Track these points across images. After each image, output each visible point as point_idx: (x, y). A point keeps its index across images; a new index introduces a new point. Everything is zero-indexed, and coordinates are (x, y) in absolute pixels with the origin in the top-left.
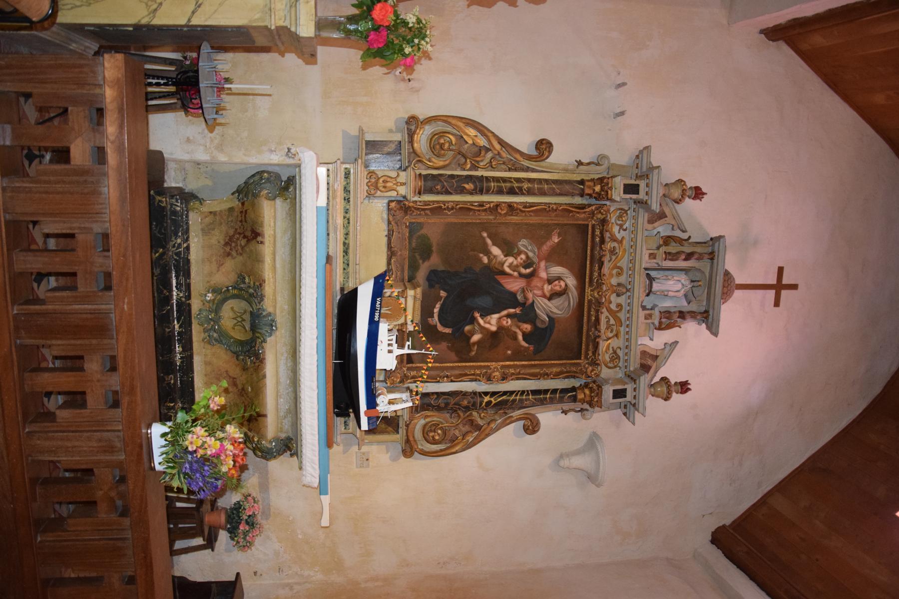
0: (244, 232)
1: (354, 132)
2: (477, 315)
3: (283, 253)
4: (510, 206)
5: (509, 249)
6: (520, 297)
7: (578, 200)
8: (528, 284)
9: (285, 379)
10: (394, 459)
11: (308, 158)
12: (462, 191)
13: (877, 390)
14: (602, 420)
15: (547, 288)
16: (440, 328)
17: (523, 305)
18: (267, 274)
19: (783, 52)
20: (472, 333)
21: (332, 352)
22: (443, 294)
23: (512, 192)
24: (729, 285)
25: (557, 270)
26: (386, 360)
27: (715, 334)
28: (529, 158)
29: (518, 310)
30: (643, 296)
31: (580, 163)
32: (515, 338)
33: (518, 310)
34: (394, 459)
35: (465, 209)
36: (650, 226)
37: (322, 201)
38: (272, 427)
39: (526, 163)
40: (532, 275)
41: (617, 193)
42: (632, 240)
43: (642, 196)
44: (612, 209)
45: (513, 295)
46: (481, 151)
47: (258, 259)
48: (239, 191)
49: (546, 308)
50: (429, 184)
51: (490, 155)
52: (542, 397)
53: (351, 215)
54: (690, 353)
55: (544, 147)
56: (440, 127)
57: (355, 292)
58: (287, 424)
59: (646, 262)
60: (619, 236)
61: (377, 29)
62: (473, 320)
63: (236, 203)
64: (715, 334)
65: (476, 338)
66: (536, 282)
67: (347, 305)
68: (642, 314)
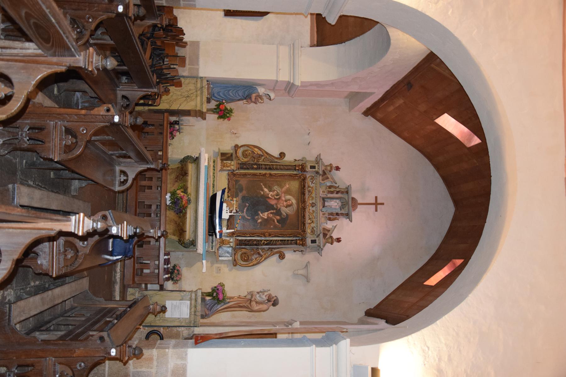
0: (182, 173)
1: (217, 151)
2: (260, 212)
3: (194, 180)
4: (270, 174)
6: (275, 206)
7: (295, 173)
8: (278, 202)
9: (193, 221)
10: (230, 270)
11: (203, 150)
12: (253, 168)
13: (433, 252)
14: (310, 256)
15: (285, 203)
16: (246, 217)
17: (276, 209)
18: (189, 185)
19: (371, 122)
20: (258, 219)
21: (208, 211)
22: (247, 204)
23: (270, 169)
24: (355, 203)
25: (288, 197)
26: (226, 215)
27: (351, 221)
28: (277, 158)
29: (275, 211)
30: (321, 207)
31: (295, 160)
32: (274, 221)
33: (275, 211)
34: (230, 270)
35: (255, 175)
36: (323, 182)
37: (206, 164)
38: (188, 236)
39: (276, 160)
40: (280, 198)
41: (308, 169)
42: (317, 189)
43: (316, 169)
44: (308, 176)
45: (273, 206)
46: (260, 156)
47: (186, 181)
48: (181, 161)
49: (285, 211)
50: (242, 166)
51: (263, 158)
52: (283, 242)
53: (215, 175)
54: (341, 228)
55: (282, 155)
56: (246, 148)
57: (216, 194)
59: (322, 194)
60: (311, 186)
61: (221, 110)
62: (258, 215)
63: (180, 165)
64: (351, 221)
66: (280, 201)
67: (214, 197)
68: (321, 213)
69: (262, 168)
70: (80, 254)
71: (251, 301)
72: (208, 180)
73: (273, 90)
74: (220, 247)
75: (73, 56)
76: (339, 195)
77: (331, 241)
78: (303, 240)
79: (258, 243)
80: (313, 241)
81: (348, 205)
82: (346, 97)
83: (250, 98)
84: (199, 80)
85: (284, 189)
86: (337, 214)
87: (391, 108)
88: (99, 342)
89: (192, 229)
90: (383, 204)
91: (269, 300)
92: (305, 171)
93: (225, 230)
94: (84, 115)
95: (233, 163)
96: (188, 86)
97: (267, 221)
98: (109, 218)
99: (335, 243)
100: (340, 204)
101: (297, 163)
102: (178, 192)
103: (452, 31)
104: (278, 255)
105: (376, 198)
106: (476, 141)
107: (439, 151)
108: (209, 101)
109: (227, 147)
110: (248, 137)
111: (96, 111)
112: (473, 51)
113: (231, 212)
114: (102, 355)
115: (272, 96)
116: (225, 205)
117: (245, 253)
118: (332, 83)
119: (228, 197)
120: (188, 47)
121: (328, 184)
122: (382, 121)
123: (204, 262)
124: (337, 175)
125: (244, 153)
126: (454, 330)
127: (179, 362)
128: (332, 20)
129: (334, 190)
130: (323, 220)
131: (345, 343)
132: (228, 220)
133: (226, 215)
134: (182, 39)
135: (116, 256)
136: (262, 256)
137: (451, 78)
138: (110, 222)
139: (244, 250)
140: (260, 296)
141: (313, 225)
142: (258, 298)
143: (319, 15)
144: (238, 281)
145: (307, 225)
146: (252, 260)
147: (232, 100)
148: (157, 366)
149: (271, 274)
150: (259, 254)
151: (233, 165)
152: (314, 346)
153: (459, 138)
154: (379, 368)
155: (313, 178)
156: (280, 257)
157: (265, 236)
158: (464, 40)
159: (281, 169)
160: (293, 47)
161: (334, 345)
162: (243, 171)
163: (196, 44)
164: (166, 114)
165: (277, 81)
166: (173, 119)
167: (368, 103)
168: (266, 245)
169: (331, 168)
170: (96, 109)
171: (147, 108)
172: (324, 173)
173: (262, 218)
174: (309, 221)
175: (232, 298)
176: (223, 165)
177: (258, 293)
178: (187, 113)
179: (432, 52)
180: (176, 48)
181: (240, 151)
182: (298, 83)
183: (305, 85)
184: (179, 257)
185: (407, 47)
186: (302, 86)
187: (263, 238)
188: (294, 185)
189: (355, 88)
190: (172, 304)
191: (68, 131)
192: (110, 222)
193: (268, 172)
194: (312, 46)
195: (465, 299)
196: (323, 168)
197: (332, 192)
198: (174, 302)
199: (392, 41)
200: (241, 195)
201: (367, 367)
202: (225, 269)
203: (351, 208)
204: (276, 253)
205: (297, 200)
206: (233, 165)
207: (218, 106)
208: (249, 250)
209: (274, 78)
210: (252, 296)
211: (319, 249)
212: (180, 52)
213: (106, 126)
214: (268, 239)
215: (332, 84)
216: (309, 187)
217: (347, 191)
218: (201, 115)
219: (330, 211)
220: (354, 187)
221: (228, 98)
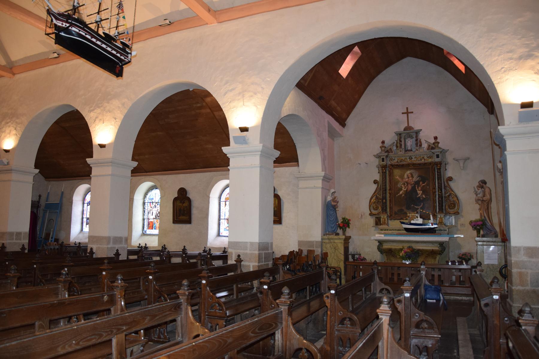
1: (374, 228)
3: (395, 244)
4: (390, 190)
5: (401, 189)
7: (388, 172)
9: (425, 245)
10: (462, 216)
11: (372, 238)
12: (386, 202)
14: (449, 158)
15: (410, 178)
17: (415, 184)
18: (399, 247)
19: (350, 121)
20: (422, 197)
21: (417, 233)
23: (386, 190)
25: (405, 176)
26: (420, 221)
28: (378, 186)
34: (462, 216)
35: (390, 201)
37: (383, 235)
38: (436, 248)
40: (407, 183)
41: (384, 163)
42: (398, 156)
45: (412, 188)
46: (377, 198)
47: (396, 249)
49: (416, 179)
52: (440, 178)
54: (426, 137)
55: (375, 182)
56: (372, 208)
58: (436, 245)
61: (344, 226)
62: (419, 197)
65: (424, 196)
67: (407, 230)
69: (386, 196)
70: (424, 318)
71: (483, 201)
72: (395, 235)
73: (329, 190)
74: (445, 225)
75: (281, 312)
76: (403, 140)
77: (436, 143)
78: (436, 164)
79: (441, 197)
80: (438, 156)
81: (410, 133)
82: (333, 140)
83: (335, 205)
84: (324, 241)
85: (400, 180)
86: (417, 140)
87: (339, 109)
88: (488, 308)
89: (431, 245)
90: (407, 108)
91: (482, 187)
92: (386, 165)
93: (432, 220)
94: (331, 312)
95: (382, 217)
96: (328, 248)
97: (424, 191)
98: (399, 298)
99: (438, 140)
100: (409, 139)
101: (381, 171)
102: (401, 255)
103: (279, 76)
104: (449, 182)
105: (403, 113)
106: (356, 49)
107: (364, 75)
108: (337, 234)
109: (371, 221)
110: (364, 207)
111: (328, 305)
112: (291, 61)
113: (417, 217)
114: (498, 305)
115: (332, 191)
116: (412, 222)
117: (449, 207)
118: (322, 150)
119: (407, 219)
120: (301, 248)
121: (395, 148)
122: (348, 114)
123: (455, 236)
124: (388, 143)
125: (374, 209)
126: (487, 51)
127: (522, 252)
128: (277, 153)
129: (399, 143)
130: (421, 150)
131: (502, 129)
132: (424, 219)
133: (420, 221)
134: (296, 252)
135: (440, 297)
136: (450, 194)
137: (314, 71)
138: (402, 297)
139: (447, 207)
140: (479, 194)
141: (426, 158)
142: (481, 195)
143: (275, 162)
144: (471, 211)
145: (426, 162)
146: (454, 201)
147: (337, 218)
148: (526, 269)
149: (463, 187)
150: (449, 196)
151: (384, 217)
152: (505, 152)
153: (355, 61)
154: (520, 103)
155: (391, 160)
156: (451, 181)
157: (435, 192)
158: (285, 68)
159: (386, 182)
160: (298, 178)
161: (504, 137)
162: (388, 210)
163: (300, 243)
164: (347, 263)
165: (322, 188)
166: (351, 259)
167: (336, 125)
168: (442, 191)
169: (383, 147)
170: (327, 305)
171: (343, 276)
172: (387, 151)
173: (422, 195)
174: (423, 160)
175: (481, 214)
176: (384, 223)
177: (477, 195)
178: (346, 249)
179: (296, 86)
180: (303, 256)
181: (374, 212)
182: (323, 174)
183: (324, 169)
184: (453, 255)
185: (293, 103)
186: (325, 171)
187: (437, 193)
188: (397, 172)
189: (325, 134)
190: (487, 259)
191: (342, 322)
192: (402, 297)
193: (388, 191)
194: (298, 165)
195: (463, 46)
196: (383, 152)
197: (401, 145)
198: (485, 257)
199: (291, 113)
200: (405, 210)
201: (520, 112)
202: (462, 220)
203: (412, 131)
204: (448, 183)
205: (407, 169)
206: (384, 217)
207: (341, 228)
208: (447, 204)
209: (320, 190)
210: (479, 200)
211: (444, 152)
212: (305, 253)
213: (338, 298)
214: (437, 190)
215: (322, 150)
216: (398, 162)
217: (399, 134)
218: (347, 240)
219: (414, 146)
220: (397, 130)
221: (335, 221)
